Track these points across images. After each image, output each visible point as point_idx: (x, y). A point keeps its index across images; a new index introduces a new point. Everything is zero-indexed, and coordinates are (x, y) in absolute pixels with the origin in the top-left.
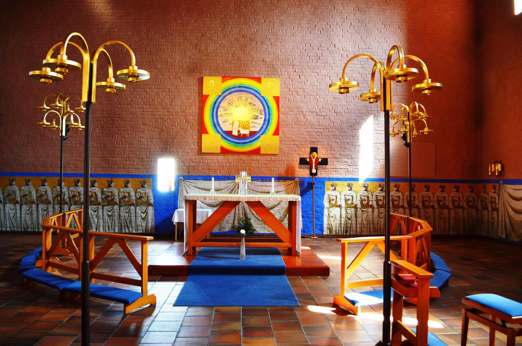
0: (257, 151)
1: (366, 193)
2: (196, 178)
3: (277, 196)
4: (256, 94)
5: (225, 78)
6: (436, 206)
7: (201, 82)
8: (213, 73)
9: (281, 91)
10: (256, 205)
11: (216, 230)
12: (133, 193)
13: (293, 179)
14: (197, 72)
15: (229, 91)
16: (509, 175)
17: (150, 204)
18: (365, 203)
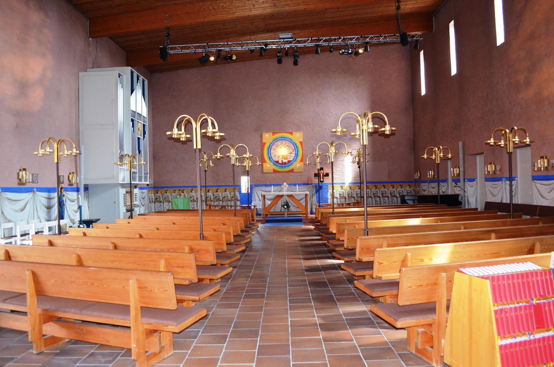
0: (292, 171)
1: (350, 191)
2: (261, 186)
3: (299, 192)
4: (291, 141)
5: (274, 133)
6: (390, 196)
7: (261, 136)
8: (268, 131)
9: (304, 139)
10: (290, 196)
11: (272, 210)
12: (229, 195)
13: (311, 184)
14: (259, 130)
15: (276, 140)
16: (422, 179)
17: (238, 200)
18: (350, 195)
